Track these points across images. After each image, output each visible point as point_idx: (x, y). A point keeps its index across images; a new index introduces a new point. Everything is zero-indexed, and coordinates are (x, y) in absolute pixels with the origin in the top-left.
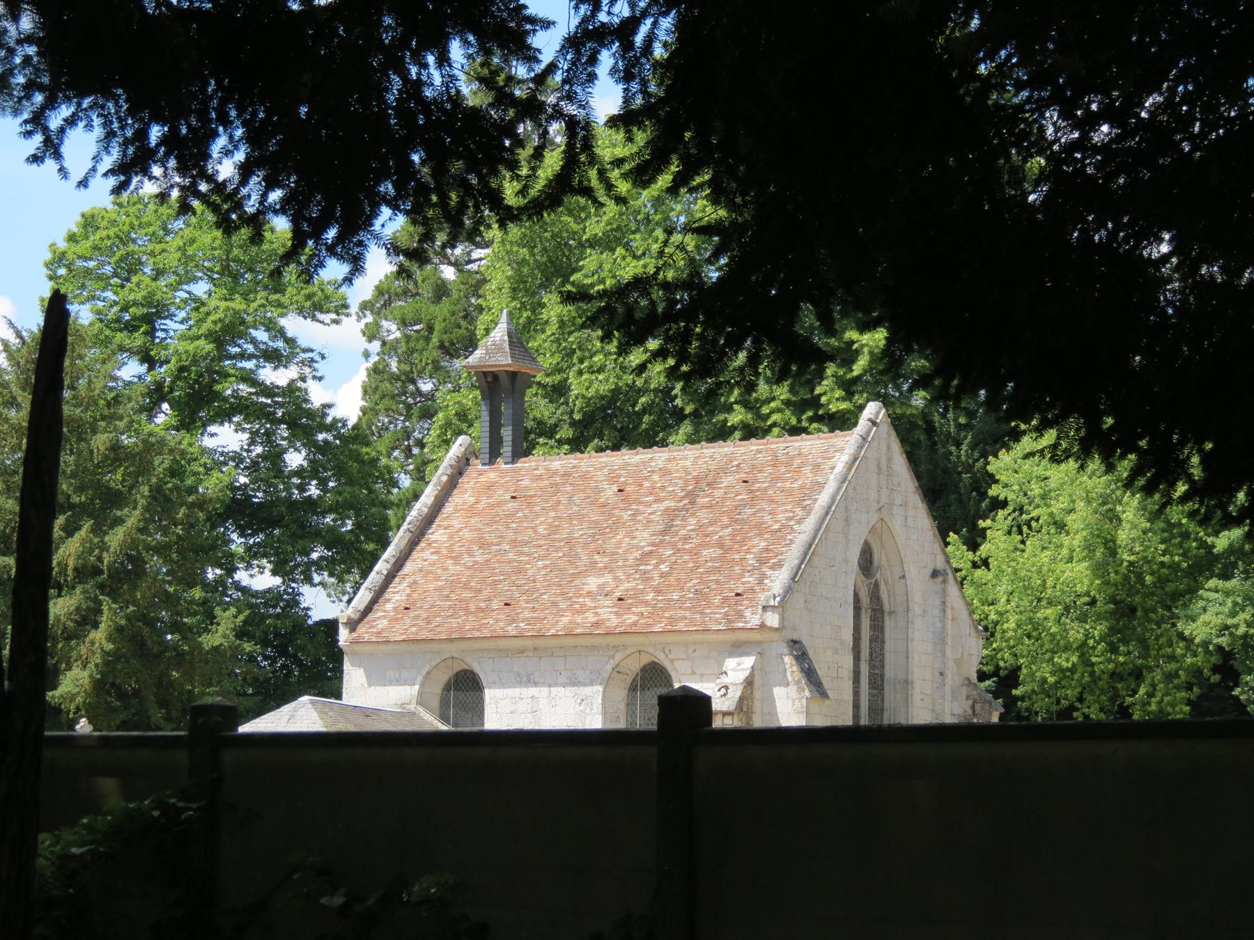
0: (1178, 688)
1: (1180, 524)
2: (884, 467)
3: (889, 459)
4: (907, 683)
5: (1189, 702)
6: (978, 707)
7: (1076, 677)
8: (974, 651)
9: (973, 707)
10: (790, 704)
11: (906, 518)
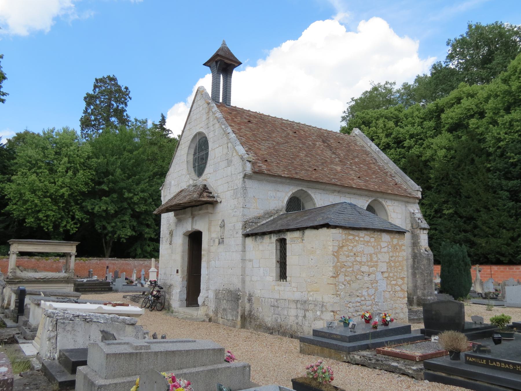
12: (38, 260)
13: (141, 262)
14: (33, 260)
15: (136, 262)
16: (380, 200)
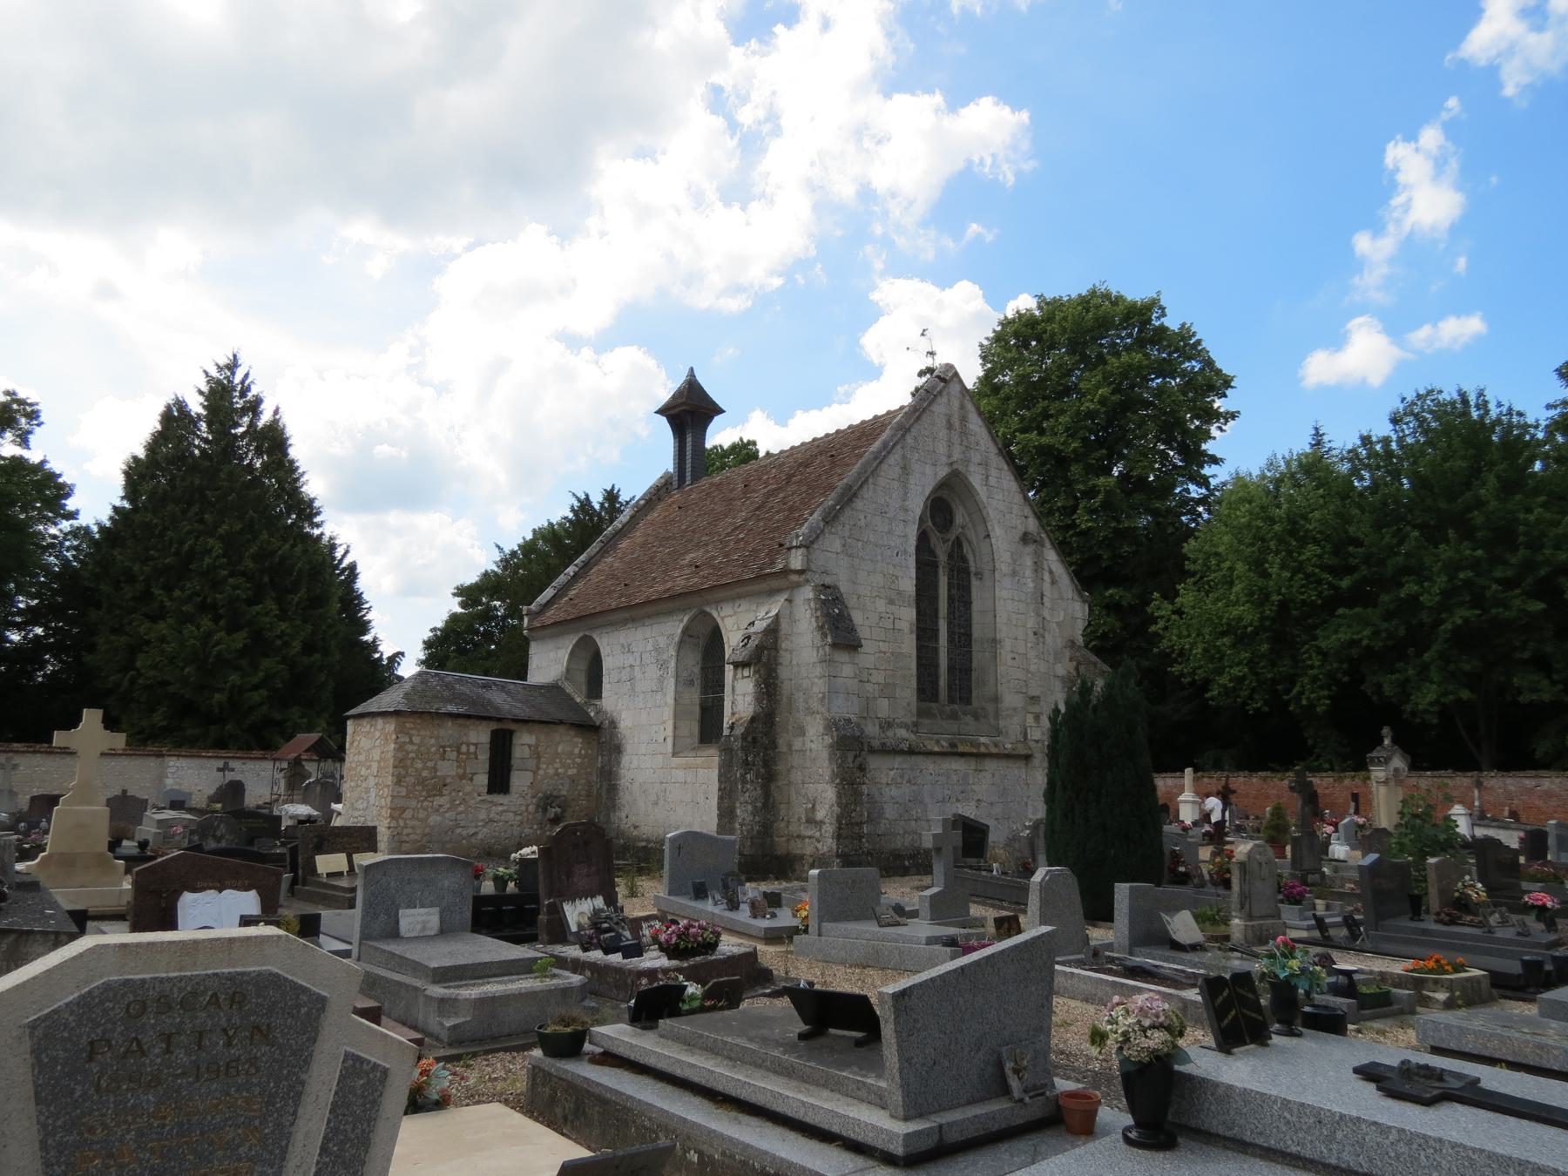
0: (1321, 688)
1: (1314, 574)
2: (957, 424)
3: (964, 419)
4: (994, 642)
5: (1329, 697)
6: (1082, 668)
7: (1247, 682)
8: (1079, 615)
9: (1077, 669)
10: (815, 653)
11: (987, 478)
12: (1265, 779)
13: (1529, 783)
14: (1254, 780)
15: (1509, 781)
16: (708, 610)
